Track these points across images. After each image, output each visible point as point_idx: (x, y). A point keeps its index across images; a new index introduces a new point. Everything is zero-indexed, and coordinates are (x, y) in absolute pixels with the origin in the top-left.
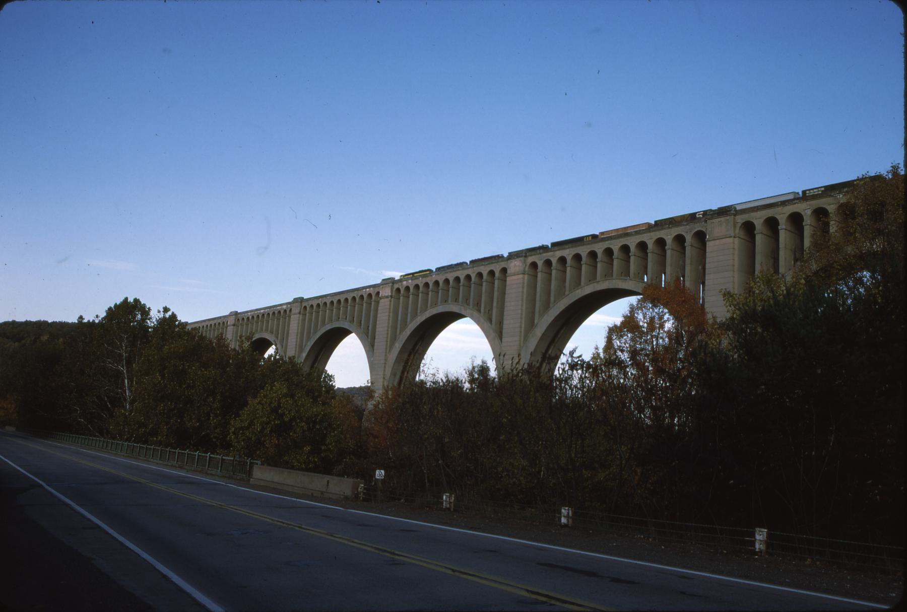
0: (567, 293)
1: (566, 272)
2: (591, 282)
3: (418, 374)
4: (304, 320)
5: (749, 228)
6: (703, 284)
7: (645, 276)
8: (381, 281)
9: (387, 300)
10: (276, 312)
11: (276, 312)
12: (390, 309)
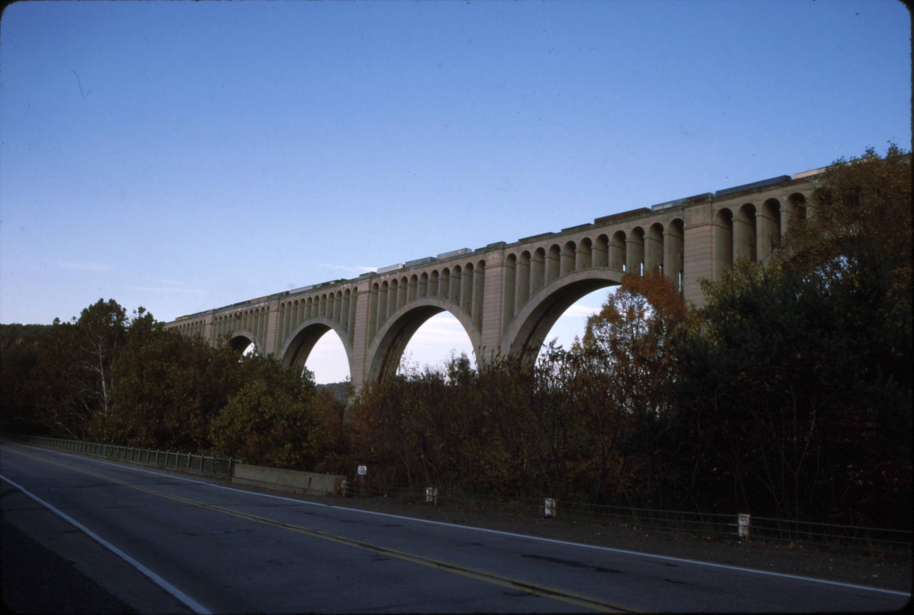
0: (546, 284)
4: (282, 317)
6: (682, 272)
10: (254, 310)
12: (368, 304)
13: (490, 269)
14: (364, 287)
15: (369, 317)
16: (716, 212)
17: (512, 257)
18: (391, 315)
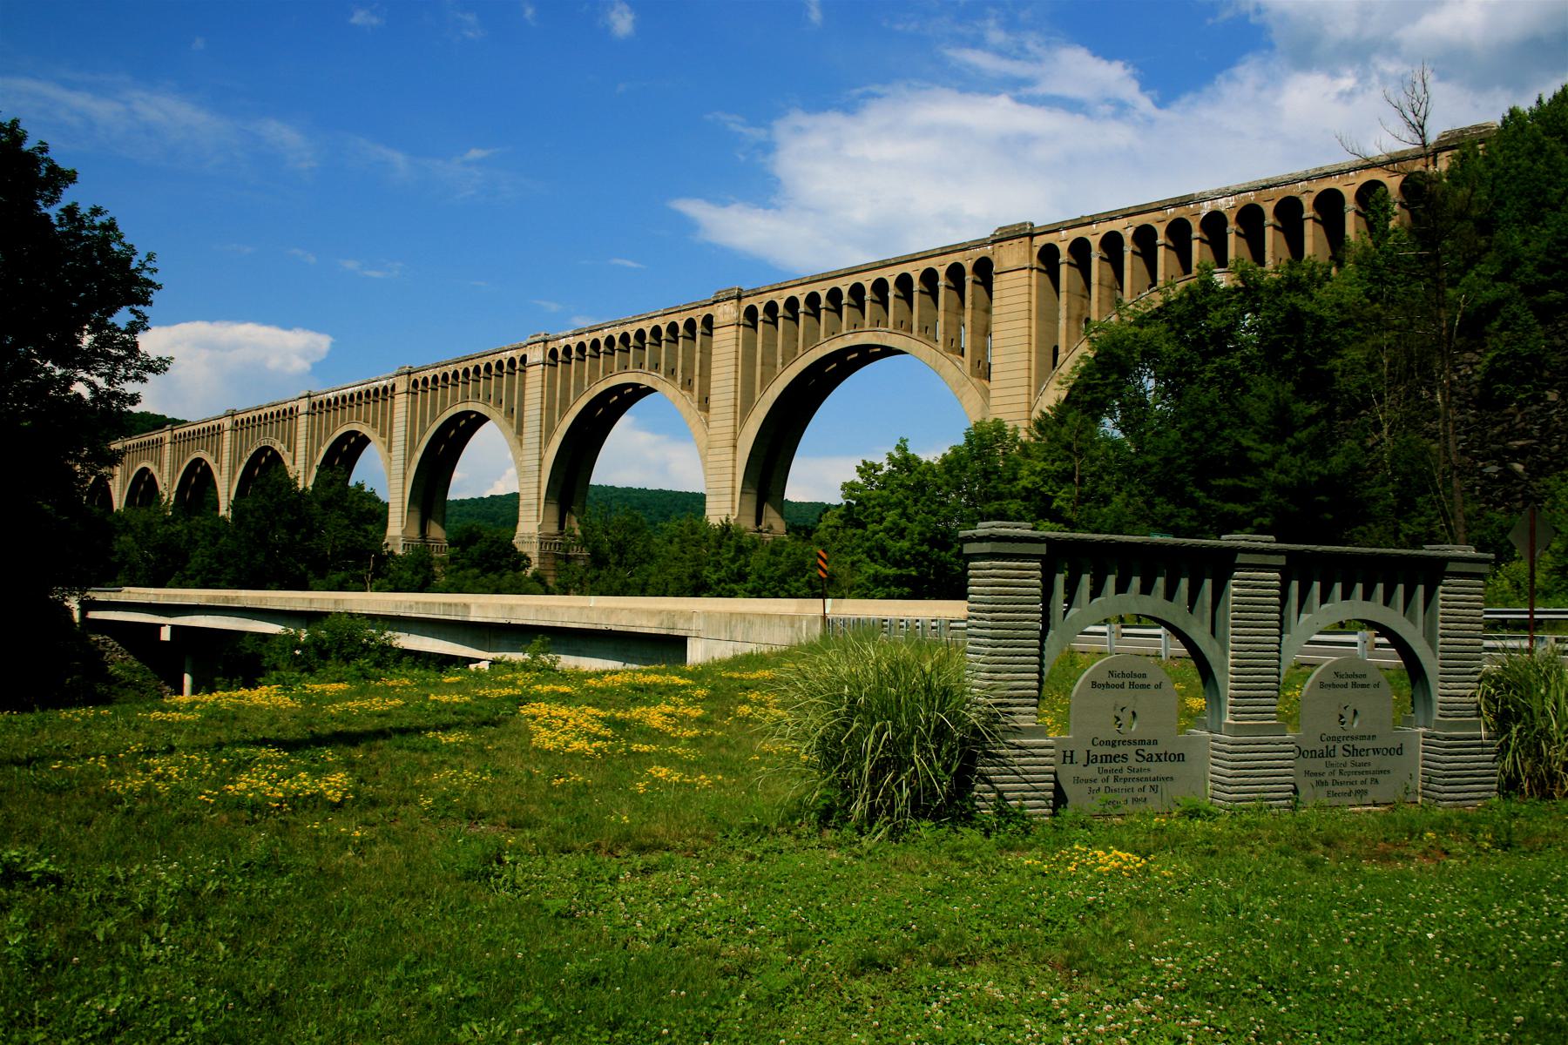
0: (800, 352)
3: (232, 498)
4: (414, 402)
5: (1049, 256)
10: (381, 389)
11: (381, 389)
17: (1049, 253)
18: (806, 350)
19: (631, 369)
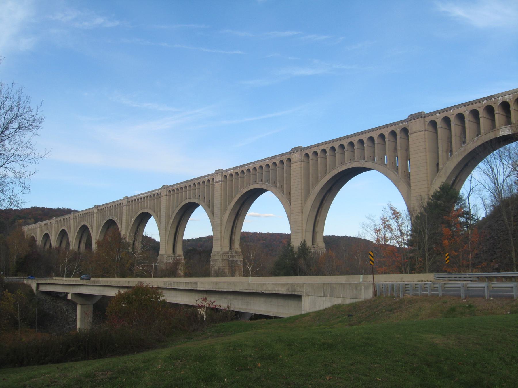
0: (328, 171)
1: (326, 158)
2: (342, 164)
5: (433, 124)
6: (409, 160)
7: (385, 156)
8: (214, 172)
9: (126, 207)
12: (221, 189)
13: (217, 183)
14: (218, 178)
15: (222, 197)
16: (427, 123)
19: (257, 182)
